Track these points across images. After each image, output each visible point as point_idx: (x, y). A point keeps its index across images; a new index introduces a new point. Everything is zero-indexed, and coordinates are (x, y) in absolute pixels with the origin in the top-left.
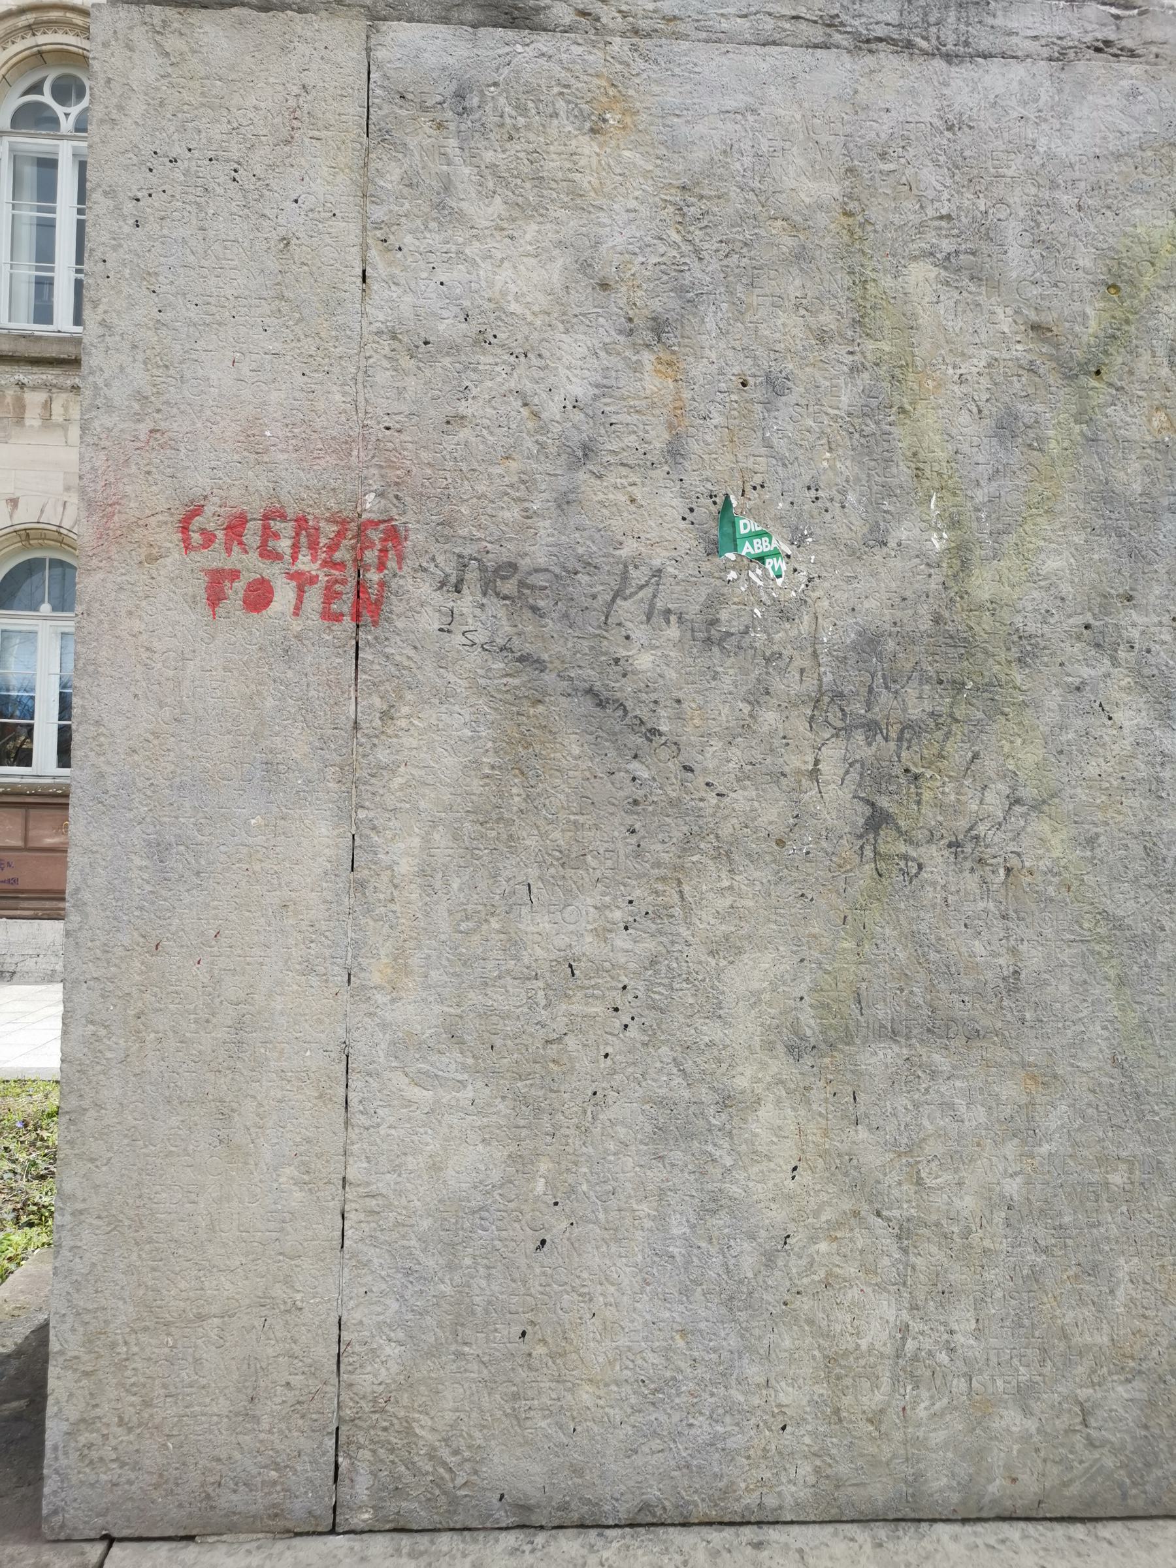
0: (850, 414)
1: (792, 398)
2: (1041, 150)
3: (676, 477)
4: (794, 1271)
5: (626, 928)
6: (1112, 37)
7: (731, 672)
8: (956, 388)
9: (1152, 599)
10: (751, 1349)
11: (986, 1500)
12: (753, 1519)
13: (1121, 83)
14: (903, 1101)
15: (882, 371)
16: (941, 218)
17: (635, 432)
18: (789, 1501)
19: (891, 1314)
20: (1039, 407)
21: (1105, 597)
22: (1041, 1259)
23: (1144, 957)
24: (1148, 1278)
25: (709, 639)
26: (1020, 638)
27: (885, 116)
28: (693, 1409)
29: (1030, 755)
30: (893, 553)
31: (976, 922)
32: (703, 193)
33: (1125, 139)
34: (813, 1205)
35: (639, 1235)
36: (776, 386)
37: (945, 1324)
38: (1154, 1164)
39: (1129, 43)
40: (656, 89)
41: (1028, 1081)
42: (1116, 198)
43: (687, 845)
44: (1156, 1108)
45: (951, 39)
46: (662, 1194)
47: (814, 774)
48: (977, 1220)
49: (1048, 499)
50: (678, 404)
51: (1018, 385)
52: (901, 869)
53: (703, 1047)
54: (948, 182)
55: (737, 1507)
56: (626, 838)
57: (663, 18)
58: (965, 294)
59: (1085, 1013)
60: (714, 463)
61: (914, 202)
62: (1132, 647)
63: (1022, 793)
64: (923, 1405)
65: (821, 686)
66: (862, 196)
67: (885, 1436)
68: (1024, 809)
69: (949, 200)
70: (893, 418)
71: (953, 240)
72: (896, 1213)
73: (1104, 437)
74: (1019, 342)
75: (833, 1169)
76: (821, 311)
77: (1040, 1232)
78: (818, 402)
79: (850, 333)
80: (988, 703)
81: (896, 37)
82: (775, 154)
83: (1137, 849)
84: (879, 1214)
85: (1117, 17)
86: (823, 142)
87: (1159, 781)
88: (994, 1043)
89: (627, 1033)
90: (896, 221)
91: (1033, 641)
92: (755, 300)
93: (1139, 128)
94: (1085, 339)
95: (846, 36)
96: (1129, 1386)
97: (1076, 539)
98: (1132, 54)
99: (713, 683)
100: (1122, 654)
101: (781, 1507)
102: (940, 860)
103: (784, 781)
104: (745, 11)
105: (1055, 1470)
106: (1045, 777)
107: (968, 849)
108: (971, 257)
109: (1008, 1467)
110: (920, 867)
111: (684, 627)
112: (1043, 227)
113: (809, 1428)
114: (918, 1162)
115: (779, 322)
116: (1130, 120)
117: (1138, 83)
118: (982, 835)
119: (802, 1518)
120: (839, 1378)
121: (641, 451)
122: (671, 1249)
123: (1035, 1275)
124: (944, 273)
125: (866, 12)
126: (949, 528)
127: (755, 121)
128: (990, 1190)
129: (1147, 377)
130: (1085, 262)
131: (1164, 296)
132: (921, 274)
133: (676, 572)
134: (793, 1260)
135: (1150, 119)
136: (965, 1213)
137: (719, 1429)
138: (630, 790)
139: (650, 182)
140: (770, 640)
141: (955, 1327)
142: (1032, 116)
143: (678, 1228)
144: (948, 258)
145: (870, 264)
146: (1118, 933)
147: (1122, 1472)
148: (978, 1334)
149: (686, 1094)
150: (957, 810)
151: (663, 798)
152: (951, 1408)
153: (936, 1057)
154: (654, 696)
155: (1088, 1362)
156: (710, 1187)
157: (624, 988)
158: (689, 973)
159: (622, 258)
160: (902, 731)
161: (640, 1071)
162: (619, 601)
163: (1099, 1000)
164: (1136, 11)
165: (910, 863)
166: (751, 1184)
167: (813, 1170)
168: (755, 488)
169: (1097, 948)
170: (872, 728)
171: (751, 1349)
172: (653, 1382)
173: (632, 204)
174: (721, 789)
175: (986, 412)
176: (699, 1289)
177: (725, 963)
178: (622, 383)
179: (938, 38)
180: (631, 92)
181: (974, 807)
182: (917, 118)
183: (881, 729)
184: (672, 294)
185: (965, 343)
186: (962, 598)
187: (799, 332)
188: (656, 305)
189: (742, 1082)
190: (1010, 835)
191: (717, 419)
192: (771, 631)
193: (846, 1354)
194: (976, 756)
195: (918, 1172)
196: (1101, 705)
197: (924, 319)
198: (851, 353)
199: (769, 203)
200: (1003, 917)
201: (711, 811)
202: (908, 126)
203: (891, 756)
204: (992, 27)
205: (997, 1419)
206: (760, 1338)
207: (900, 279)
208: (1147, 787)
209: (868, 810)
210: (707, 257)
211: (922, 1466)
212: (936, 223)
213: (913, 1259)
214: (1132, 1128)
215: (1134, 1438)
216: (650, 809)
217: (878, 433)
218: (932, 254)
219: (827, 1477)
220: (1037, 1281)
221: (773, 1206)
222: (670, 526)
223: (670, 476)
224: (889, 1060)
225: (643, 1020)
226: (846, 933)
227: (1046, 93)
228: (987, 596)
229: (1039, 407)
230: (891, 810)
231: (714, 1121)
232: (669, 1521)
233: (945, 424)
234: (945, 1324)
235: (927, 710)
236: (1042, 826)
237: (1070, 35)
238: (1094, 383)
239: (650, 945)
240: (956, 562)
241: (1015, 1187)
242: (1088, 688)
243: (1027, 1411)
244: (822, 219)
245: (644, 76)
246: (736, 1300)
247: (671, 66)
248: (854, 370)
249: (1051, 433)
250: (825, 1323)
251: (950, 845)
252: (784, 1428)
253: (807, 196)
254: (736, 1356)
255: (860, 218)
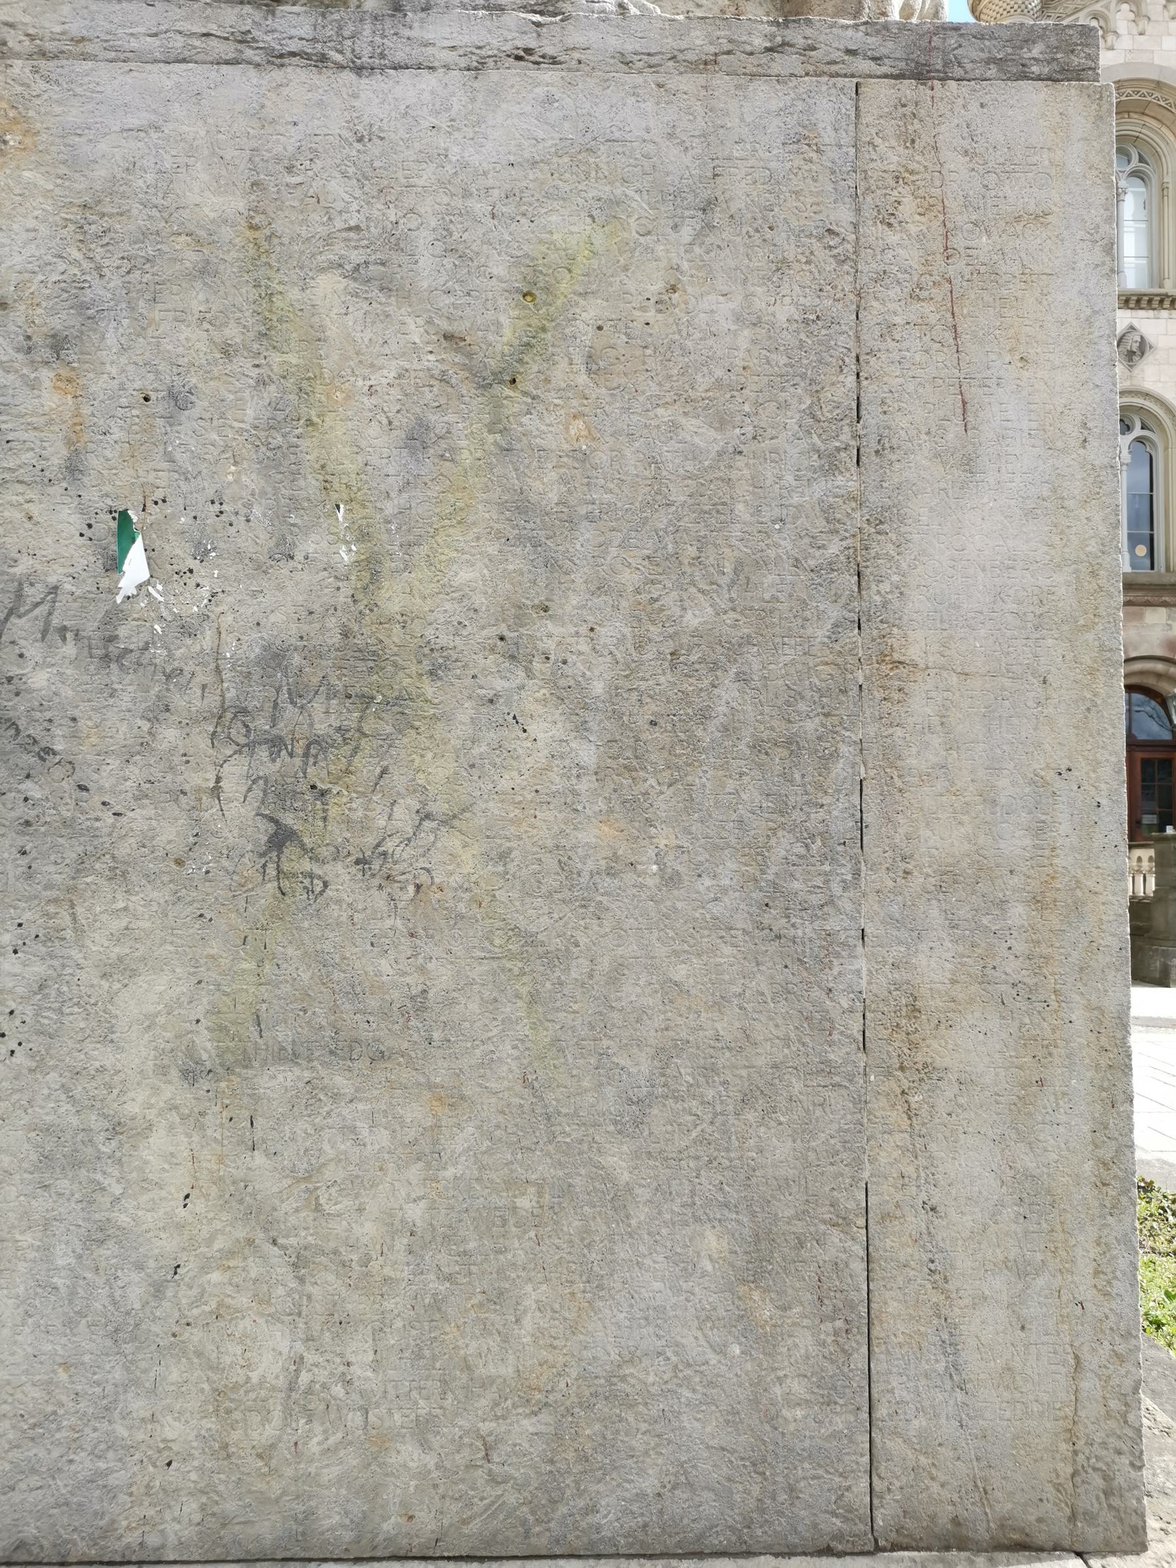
0: (256, 427)
1: (195, 412)
2: (454, 159)
3: (73, 493)
4: (184, 1301)
5: (15, 952)
6: (532, 44)
7: (130, 689)
8: (365, 400)
9: (568, 608)
10: (136, 1382)
11: (381, 1537)
12: (134, 1559)
13: (536, 90)
14: (302, 1125)
15: (290, 384)
16: (350, 229)
17: (33, 449)
18: (172, 1539)
19: (284, 1346)
20: (451, 418)
21: (520, 608)
22: (444, 1287)
23: (557, 974)
24: (557, 1306)
25: (107, 656)
26: (432, 650)
27: (292, 129)
28: (75, 1444)
29: (439, 770)
30: (300, 567)
31: (383, 940)
32: (105, 210)
33: (540, 146)
34: (205, 1234)
35: (22, 1267)
36: (179, 400)
37: (341, 1355)
38: (565, 1187)
39: (550, 50)
40: (57, 109)
41: (434, 1103)
42: (531, 205)
43: (81, 866)
44: (567, 1129)
45: (366, 52)
46: (46, 1226)
47: (216, 791)
48: (378, 1247)
49: (461, 509)
50: (77, 420)
51: (429, 396)
52: (305, 888)
53: (93, 1072)
54: (358, 193)
55: (118, 1546)
56: (16, 859)
57: (72, 40)
58: (374, 305)
59: (495, 1032)
60: (113, 479)
61: (322, 214)
62: (548, 658)
63: (432, 808)
64: (315, 1440)
65: (223, 702)
66: (269, 210)
67: (273, 1472)
68: (434, 824)
69: (358, 211)
70: (300, 430)
71: (361, 251)
72: (293, 1241)
73: (518, 446)
74: (431, 352)
75: (227, 1196)
76: (226, 324)
77: (443, 1258)
78: (222, 416)
79: (256, 346)
80: (398, 716)
81: (309, 51)
82: (179, 170)
83: (550, 862)
84: (274, 1242)
85: (538, 24)
86: (228, 157)
87: (575, 793)
88: (399, 1064)
89: (14, 1059)
90: (304, 233)
91: (445, 654)
92: (157, 315)
93: (557, 136)
94: (499, 348)
95: (257, 52)
96: (534, 1419)
97: (490, 550)
98: (554, 61)
99: (111, 701)
100: (537, 665)
101: (163, 1546)
102: (348, 877)
103: (183, 799)
104: (155, 30)
105: (455, 1507)
106: (456, 791)
107: (376, 865)
108: (382, 269)
109: (404, 1504)
110: (326, 884)
111: (80, 645)
112: (456, 236)
113: (196, 1463)
114: (316, 1189)
115: (182, 337)
116: (546, 126)
117: (553, 90)
118: (390, 851)
119: (185, 1558)
120: (228, 1412)
121: (39, 467)
122: (55, 1280)
123: (438, 1304)
124: (353, 285)
125: (280, 28)
126: (358, 540)
127: (159, 138)
128: (391, 1216)
129: (563, 385)
130: (499, 270)
131: (582, 302)
132: (328, 288)
133: (74, 589)
134: (183, 1291)
135: (567, 125)
136: (364, 1240)
137: (102, 1465)
138: (22, 811)
139: (50, 201)
140: (170, 655)
141: (352, 1359)
142: (444, 126)
143: (63, 1258)
144: (357, 268)
145: (278, 277)
146: (530, 949)
147: (525, 1509)
148: (376, 1365)
149: (75, 1121)
150: (365, 826)
151: (57, 818)
152: (345, 1443)
153: (339, 1080)
154: (48, 715)
155: (491, 1394)
156: (97, 1216)
157: (12, 1013)
158: (81, 997)
159: (21, 277)
160: (308, 747)
161: (26, 1097)
162: (13, 619)
163: (510, 1019)
164: (559, 18)
165: (315, 881)
166: (140, 1213)
167: (206, 1196)
168: (156, 503)
169: (509, 965)
170: (276, 744)
171: (136, 1382)
172: (33, 1417)
173: (31, 223)
174: (118, 809)
175: (396, 423)
176: (84, 1321)
177: (119, 986)
178: (18, 401)
179: (353, 50)
180: (31, 113)
181: (382, 823)
182: (326, 131)
183: (286, 745)
184: (72, 311)
185: (374, 356)
186: (371, 610)
187: (202, 346)
188: (56, 323)
189: (133, 1108)
190: (421, 850)
191: (117, 434)
192: (172, 647)
193: (236, 1387)
194: (384, 771)
195: (317, 1198)
196: (514, 718)
197: (332, 332)
198: (257, 366)
199: (172, 219)
200: (412, 935)
201: (106, 830)
202: (317, 139)
203: (296, 773)
204: (408, 39)
205: (394, 1454)
206: (145, 1371)
207: (308, 292)
208: (563, 800)
209: (271, 828)
210: (108, 274)
211: (313, 1503)
212: (345, 234)
213: (309, 1288)
214: (542, 1150)
215: (539, 1474)
216: (43, 829)
217: (285, 446)
218: (340, 265)
219: (213, 1514)
220: (439, 1309)
221: (163, 1235)
222: (67, 542)
223: (68, 492)
224: (289, 1084)
225: (31, 1045)
226: (246, 953)
227: (459, 102)
228: (397, 609)
229: (451, 418)
230: (295, 827)
231: (104, 1149)
232: (45, 1560)
233: (357, 437)
234: (341, 1355)
235: (334, 724)
236: (451, 841)
237: (489, 44)
238: (507, 392)
239: (38, 969)
240: (366, 575)
241: (419, 1212)
242: (501, 700)
243: (424, 1445)
244: (226, 233)
245: (45, 96)
246: (122, 1332)
247: (73, 86)
248: (262, 382)
249: (464, 443)
250: (214, 1355)
251: (357, 862)
252: (169, 1464)
253: (212, 211)
254: (121, 1390)
255: (267, 232)
